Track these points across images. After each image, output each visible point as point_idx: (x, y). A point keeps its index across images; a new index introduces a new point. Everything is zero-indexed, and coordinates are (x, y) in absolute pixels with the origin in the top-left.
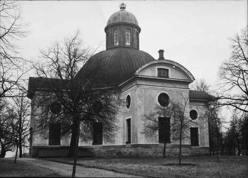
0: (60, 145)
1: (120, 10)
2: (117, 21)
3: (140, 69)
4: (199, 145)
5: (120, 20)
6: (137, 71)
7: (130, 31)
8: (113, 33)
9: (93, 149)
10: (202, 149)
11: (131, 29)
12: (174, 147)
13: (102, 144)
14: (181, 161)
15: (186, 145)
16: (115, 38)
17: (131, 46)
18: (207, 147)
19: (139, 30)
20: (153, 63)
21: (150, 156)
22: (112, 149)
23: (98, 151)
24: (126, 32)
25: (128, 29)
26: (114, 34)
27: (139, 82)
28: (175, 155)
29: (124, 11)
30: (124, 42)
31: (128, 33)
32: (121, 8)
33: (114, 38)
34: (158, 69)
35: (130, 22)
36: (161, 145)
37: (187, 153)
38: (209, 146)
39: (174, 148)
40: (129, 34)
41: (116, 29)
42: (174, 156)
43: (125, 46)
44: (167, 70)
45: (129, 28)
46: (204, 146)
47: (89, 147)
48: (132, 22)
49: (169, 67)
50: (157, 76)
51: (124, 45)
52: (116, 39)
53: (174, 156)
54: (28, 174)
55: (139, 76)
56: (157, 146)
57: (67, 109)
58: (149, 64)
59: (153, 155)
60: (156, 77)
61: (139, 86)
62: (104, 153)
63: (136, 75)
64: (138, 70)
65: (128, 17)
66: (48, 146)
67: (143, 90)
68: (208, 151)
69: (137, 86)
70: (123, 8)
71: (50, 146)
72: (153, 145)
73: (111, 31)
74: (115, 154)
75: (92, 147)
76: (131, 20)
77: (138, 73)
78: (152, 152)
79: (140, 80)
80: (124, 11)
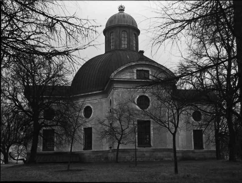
0: (54, 150)
1: (119, 12)
2: (113, 24)
3: (115, 72)
4: (203, 148)
5: (116, 23)
6: (113, 74)
7: (126, 33)
8: (109, 36)
9: (83, 154)
10: (207, 152)
11: (128, 31)
12: (154, 151)
13: (92, 149)
14: (70, 167)
15: (169, 149)
16: (112, 41)
17: (127, 48)
18: (214, 151)
19: (138, 32)
20: (130, 65)
21: (128, 161)
22: (101, 154)
23: (89, 156)
24: (122, 35)
25: (125, 31)
26: (110, 37)
27: (115, 86)
28: (156, 159)
29: (123, 14)
30: (120, 44)
31: (124, 35)
32: (119, 10)
33: (110, 41)
34: (137, 71)
35: (126, 24)
36: (139, 149)
37: (170, 157)
38: (215, 150)
39: (155, 152)
40: (125, 37)
41: (113, 32)
42: (154, 160)
43: (121, 49)
44: (148, 71)
45: (125, 30)
46: (209, 150)
47: (80, 153)
48: (128, 24)
49: (149, 68)
50: (135, 78)
51: (120, 48)
52: (113, 42)
53: (154, 160)
54: (192, 174)
55: (115, 80)
56: (98, 152)
57: (214, 114)
58: (125, 67)
59: (131, 160)
60: (135, 79)
61: (115, 89)
62: (94, 158)
63: (112, 78)
64: (113, 73)
65: (124, 19)
66: (41, 153)
67: (120, 93)
68: (214, 155)
69: (114, 90)
70: (121, 9)
71: (44, 152)
72: (131, 149)
73: (108, 35)
74: (103, 160)
75: (82, 153)
76: (127, 22)
77: (113, 76)
78: (130, 157)
79: (117, 83)
80: (123, 13)
